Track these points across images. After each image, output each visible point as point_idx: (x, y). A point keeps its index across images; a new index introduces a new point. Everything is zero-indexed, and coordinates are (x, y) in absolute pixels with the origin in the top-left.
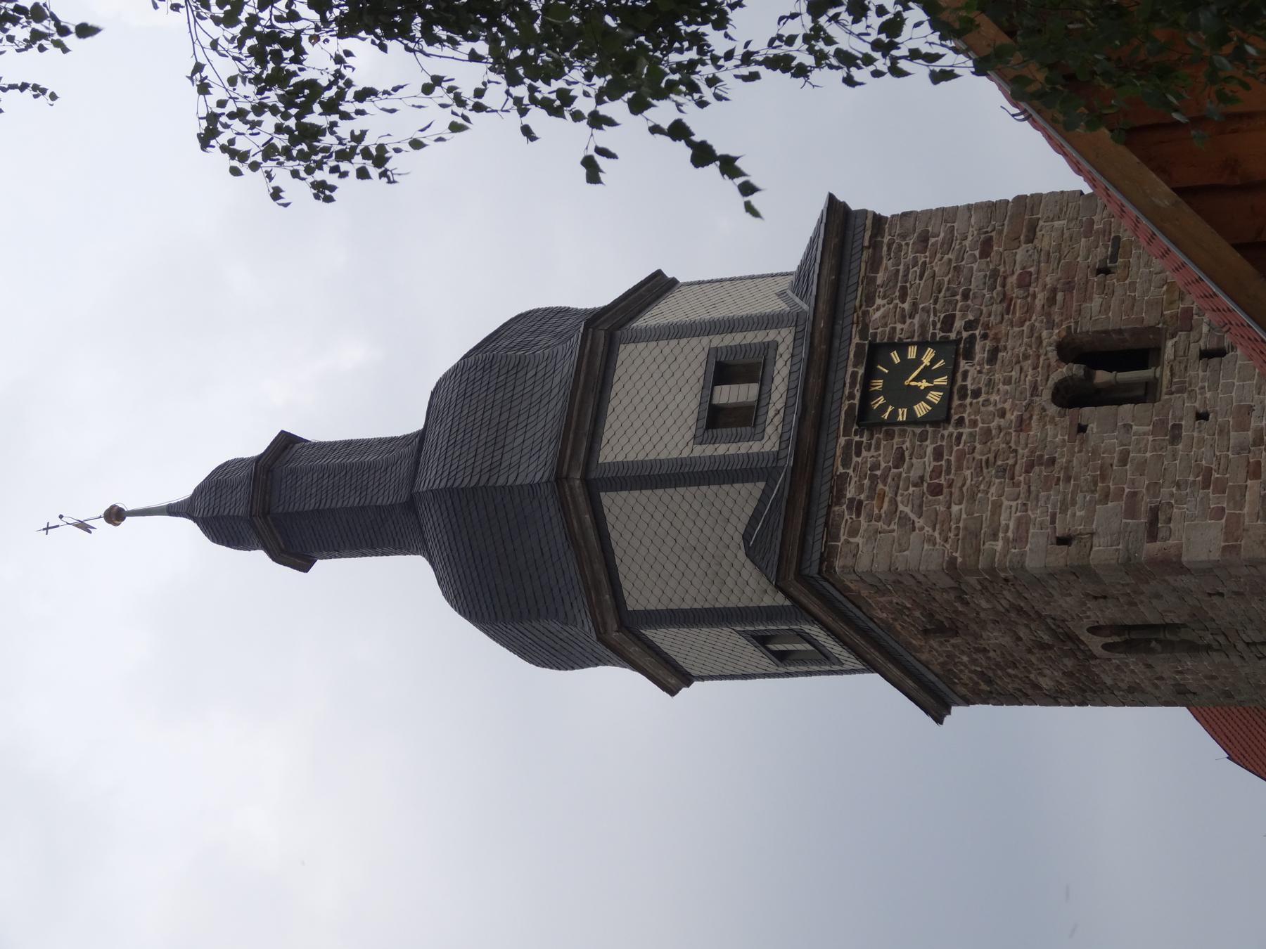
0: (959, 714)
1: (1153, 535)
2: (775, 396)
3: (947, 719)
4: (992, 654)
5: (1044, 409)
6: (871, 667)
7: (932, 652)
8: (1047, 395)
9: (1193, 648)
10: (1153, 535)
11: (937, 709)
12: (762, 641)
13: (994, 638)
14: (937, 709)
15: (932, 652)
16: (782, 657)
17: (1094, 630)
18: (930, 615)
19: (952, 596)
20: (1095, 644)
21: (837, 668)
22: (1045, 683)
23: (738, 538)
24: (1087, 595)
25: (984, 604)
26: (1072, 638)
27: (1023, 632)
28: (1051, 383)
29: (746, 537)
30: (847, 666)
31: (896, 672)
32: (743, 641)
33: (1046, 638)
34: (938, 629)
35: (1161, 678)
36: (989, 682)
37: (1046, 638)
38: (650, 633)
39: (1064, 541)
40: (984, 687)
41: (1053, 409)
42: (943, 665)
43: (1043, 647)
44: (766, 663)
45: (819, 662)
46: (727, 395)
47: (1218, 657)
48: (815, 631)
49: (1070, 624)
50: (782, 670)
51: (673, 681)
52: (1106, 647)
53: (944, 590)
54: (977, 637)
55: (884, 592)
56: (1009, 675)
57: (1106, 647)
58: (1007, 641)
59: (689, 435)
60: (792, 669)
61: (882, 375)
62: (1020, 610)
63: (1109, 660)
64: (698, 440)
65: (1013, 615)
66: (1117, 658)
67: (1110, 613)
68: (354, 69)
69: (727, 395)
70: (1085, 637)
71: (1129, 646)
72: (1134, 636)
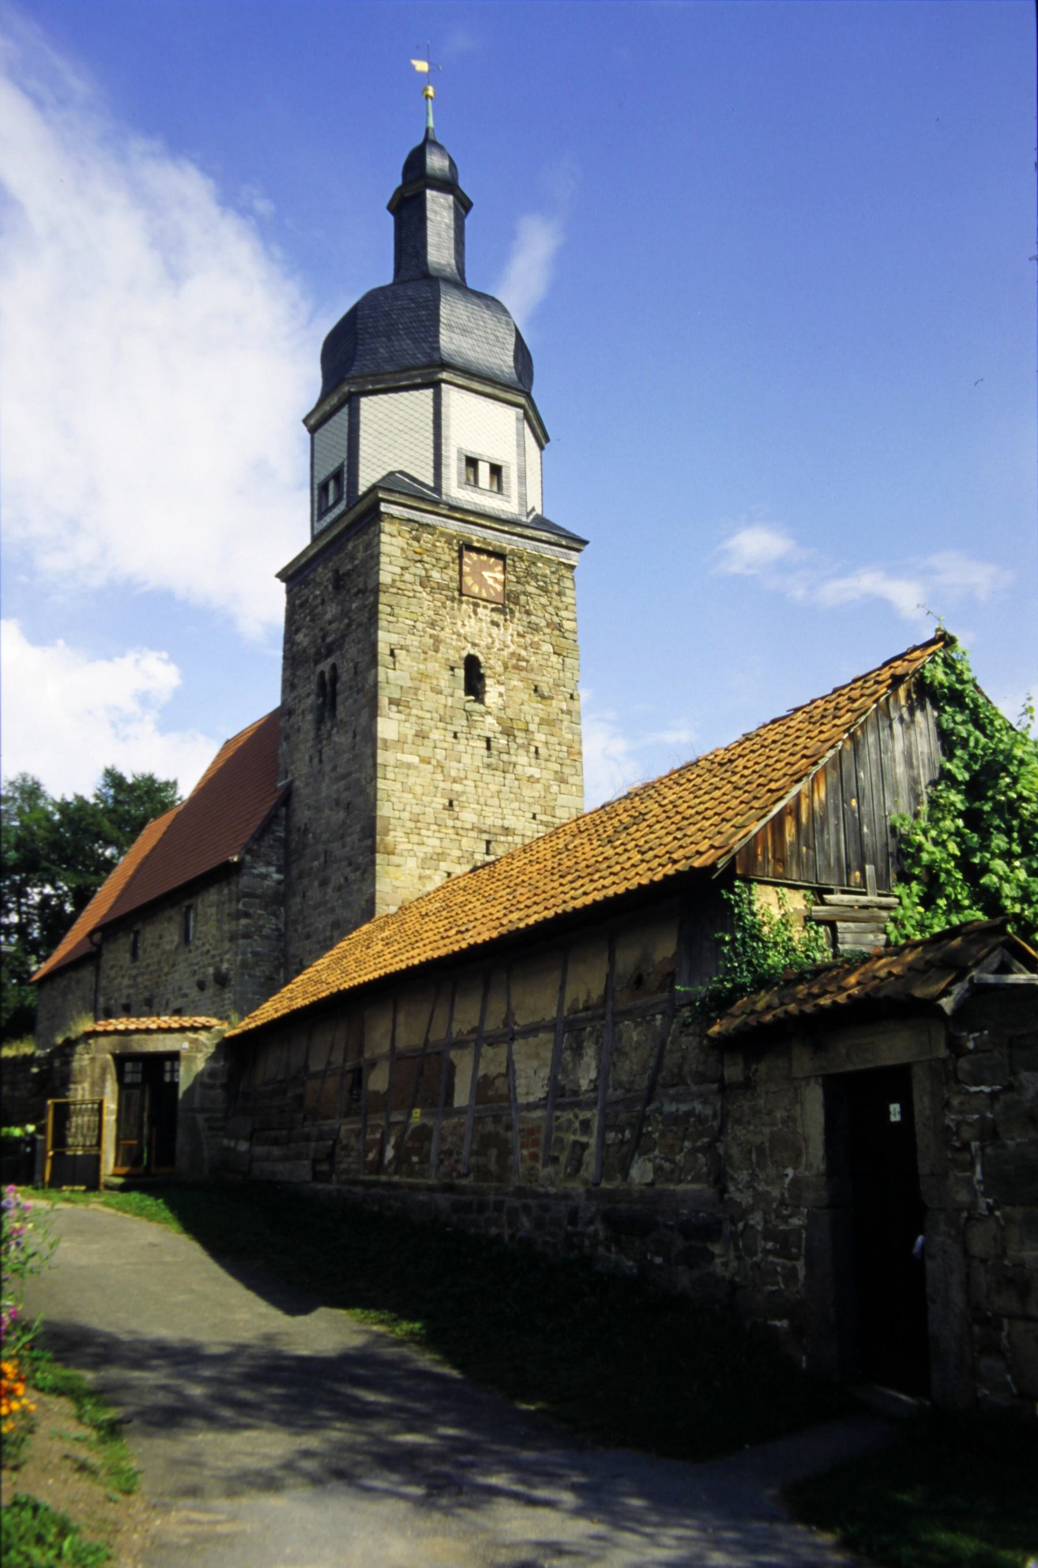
0: (283, 586)
1: (392, 702)
2: (482, 498)
3: (278, 580)
4: (320, 607)
5: (464, 649)
6: (315, 538)
7: (323, 574)
8: (472, 652)
9: (319, 721)
10: (392, 702)
11: (284, 575)
12: (337, 476)
13: (332, 610)
14: (284, 575)
15: (323, 574)
16: (324, 488)
17: (334, 667)
18: (348, 574)
19: (361, 586)
20: (325, 666)
21: (316, 518)
22: (299, 637)
23: (401, 468)
24: (357, 663)
25: (354, 606)
26: (330, 652)
27: (334, 626)
28: (478, 654)
29: (401, 472)
30: (316, 525)
31: (311, 553)
32: (337, 465)
33: (329, 640)
34: (339, 581)
35: (300, 701)
36: (301, 606)
37: (329, 640)
38: (345, 410)
39: (392, 654)
40: (298, 602)
41: (464, 654)
42: (314, 580)
43: (324, 638)
44: (320, 477)
45: (319, 508)
46: (484, 470)
47: (312, 734)
48: (342, 507)
49: (338, 653)
50: (316, 486)
51: (312, 422)
52: (322, 674)
53: (365, 583)
54: (332, 600)
55: (366, 549)
56: (305, 617)
57: (322, 674)
58: (329, 616)
59: (463, 446)
60: (316, 492)
61: (468, 565)
62: (349, 625)
63: (314, 673)
64: (460, 451)
65: (346, 621)
66: (314, 679)
67: (345, 676)
68: (428, 140)
69: (484, 470)
70: (330, 661)
71: (322, 684)
72: (329, 688)
